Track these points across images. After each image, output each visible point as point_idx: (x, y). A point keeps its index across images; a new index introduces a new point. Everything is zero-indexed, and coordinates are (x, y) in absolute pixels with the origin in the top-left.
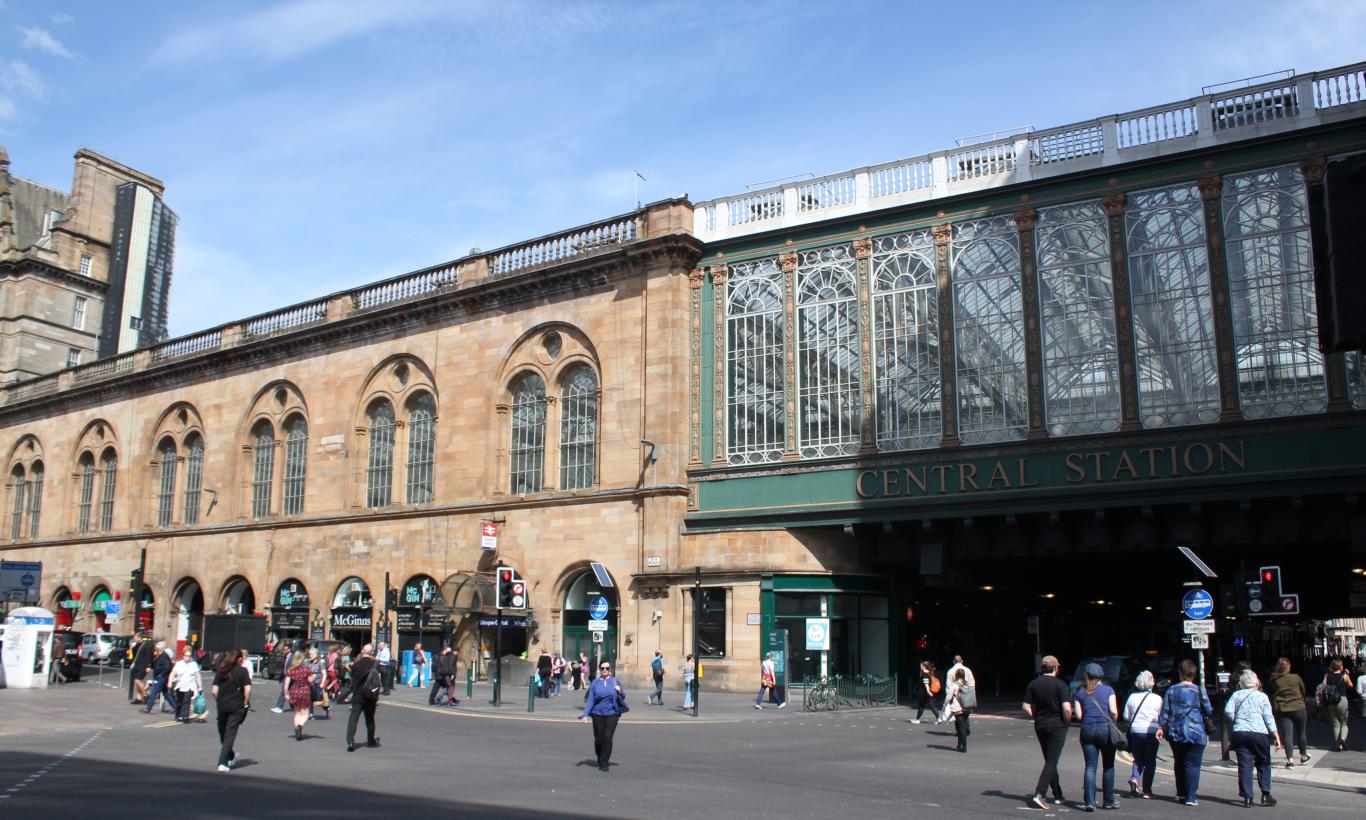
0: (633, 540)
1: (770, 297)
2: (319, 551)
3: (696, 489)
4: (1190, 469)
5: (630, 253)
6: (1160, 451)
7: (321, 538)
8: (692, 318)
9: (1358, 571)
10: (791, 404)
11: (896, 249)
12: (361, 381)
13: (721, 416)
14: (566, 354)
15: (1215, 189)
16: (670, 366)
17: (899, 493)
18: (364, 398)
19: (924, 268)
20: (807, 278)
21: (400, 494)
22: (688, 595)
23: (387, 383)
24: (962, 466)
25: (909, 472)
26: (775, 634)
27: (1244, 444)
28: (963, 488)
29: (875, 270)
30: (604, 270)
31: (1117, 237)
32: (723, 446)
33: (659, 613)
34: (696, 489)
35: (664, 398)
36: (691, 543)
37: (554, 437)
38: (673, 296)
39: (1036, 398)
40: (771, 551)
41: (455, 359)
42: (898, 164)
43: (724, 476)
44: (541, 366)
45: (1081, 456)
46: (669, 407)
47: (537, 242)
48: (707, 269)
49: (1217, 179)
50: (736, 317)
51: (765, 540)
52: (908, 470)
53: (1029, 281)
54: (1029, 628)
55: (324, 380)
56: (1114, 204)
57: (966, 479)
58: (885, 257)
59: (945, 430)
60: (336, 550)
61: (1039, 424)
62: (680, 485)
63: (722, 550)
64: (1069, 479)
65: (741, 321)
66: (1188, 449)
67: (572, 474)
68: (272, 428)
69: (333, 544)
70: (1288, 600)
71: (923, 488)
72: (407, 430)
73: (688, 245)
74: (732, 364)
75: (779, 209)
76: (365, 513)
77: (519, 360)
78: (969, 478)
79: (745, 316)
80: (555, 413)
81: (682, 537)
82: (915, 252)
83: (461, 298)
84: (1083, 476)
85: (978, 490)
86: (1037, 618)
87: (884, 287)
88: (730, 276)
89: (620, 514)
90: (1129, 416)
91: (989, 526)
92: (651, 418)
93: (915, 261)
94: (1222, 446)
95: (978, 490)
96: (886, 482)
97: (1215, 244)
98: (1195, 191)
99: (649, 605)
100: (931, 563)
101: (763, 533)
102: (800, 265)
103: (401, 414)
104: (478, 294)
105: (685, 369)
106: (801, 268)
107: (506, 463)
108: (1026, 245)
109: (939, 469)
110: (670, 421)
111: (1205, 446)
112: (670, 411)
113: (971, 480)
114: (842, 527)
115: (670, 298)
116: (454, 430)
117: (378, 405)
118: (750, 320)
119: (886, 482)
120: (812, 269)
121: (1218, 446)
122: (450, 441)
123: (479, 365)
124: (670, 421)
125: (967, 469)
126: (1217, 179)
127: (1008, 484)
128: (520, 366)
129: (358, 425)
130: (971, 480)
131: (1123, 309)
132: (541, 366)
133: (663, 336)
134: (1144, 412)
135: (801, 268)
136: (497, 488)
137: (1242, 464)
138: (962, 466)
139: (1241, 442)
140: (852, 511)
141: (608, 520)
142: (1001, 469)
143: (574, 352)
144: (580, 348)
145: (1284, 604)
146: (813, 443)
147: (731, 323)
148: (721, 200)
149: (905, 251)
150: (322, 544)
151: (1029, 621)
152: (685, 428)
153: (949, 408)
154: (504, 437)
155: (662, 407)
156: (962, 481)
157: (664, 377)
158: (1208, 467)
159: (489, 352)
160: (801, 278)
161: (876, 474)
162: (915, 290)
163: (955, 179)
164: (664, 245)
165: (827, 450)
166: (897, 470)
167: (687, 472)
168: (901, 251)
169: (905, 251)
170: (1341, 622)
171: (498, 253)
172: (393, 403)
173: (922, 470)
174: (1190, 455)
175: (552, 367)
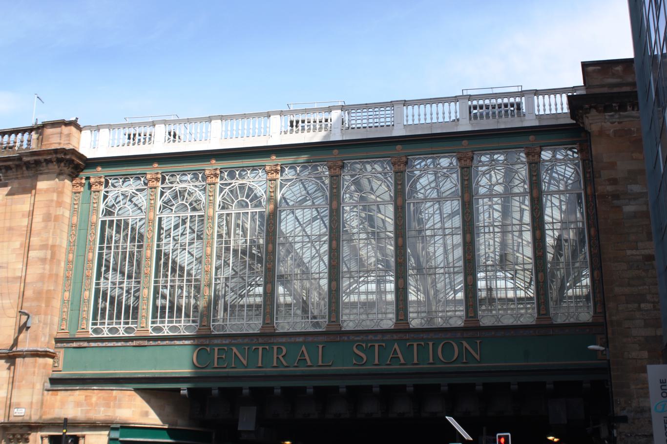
3: (61, 354)
4: (442, 359)
8: (72, 215)
15: (468, 160)
16: (49, 252)
25: (235, 350)
27: (248, 348)
28: (275, 364)
29: (161, 197)
31: (399, 187)
34: (61, 354)
35: (42, 278)
36: (53, 398)
38: (58, 197)
39: (268, 303)
40: (120, 407)
45: (364, 345)
48: (88, 178)
50: (108, 218)
53: (536, 202)
57: (278, 358)
59: (330, 317)
63: (78, 404)
64: (354, 362)
66: (444, 342)
78: (280, 357)
81: (46, 392)
91: (292, 395)
92: (29, 293)
94: (465, 344)
101: (115, 392)
102: (163, 183)
105: (62, 256)
111: (453, 343)
119: (216, 356)
120: (230, 184)
124: (45, 297)
125: (279, 350)
126: (470, 154)
127: (309, 363)
131: (468, 236)
134: (411, 315)
135: (164, 186)
138: (275, 348)
146: (117, 323)
147: (103, 223)
148: (275, 113)
152: (57, 303)
153: (268, 303)
155: (39, 285)
160: (162, 193)
161: (208, 349)
166: (226, 348)
167: (55, 339)
169: (244, 182)
173: (245, 348)
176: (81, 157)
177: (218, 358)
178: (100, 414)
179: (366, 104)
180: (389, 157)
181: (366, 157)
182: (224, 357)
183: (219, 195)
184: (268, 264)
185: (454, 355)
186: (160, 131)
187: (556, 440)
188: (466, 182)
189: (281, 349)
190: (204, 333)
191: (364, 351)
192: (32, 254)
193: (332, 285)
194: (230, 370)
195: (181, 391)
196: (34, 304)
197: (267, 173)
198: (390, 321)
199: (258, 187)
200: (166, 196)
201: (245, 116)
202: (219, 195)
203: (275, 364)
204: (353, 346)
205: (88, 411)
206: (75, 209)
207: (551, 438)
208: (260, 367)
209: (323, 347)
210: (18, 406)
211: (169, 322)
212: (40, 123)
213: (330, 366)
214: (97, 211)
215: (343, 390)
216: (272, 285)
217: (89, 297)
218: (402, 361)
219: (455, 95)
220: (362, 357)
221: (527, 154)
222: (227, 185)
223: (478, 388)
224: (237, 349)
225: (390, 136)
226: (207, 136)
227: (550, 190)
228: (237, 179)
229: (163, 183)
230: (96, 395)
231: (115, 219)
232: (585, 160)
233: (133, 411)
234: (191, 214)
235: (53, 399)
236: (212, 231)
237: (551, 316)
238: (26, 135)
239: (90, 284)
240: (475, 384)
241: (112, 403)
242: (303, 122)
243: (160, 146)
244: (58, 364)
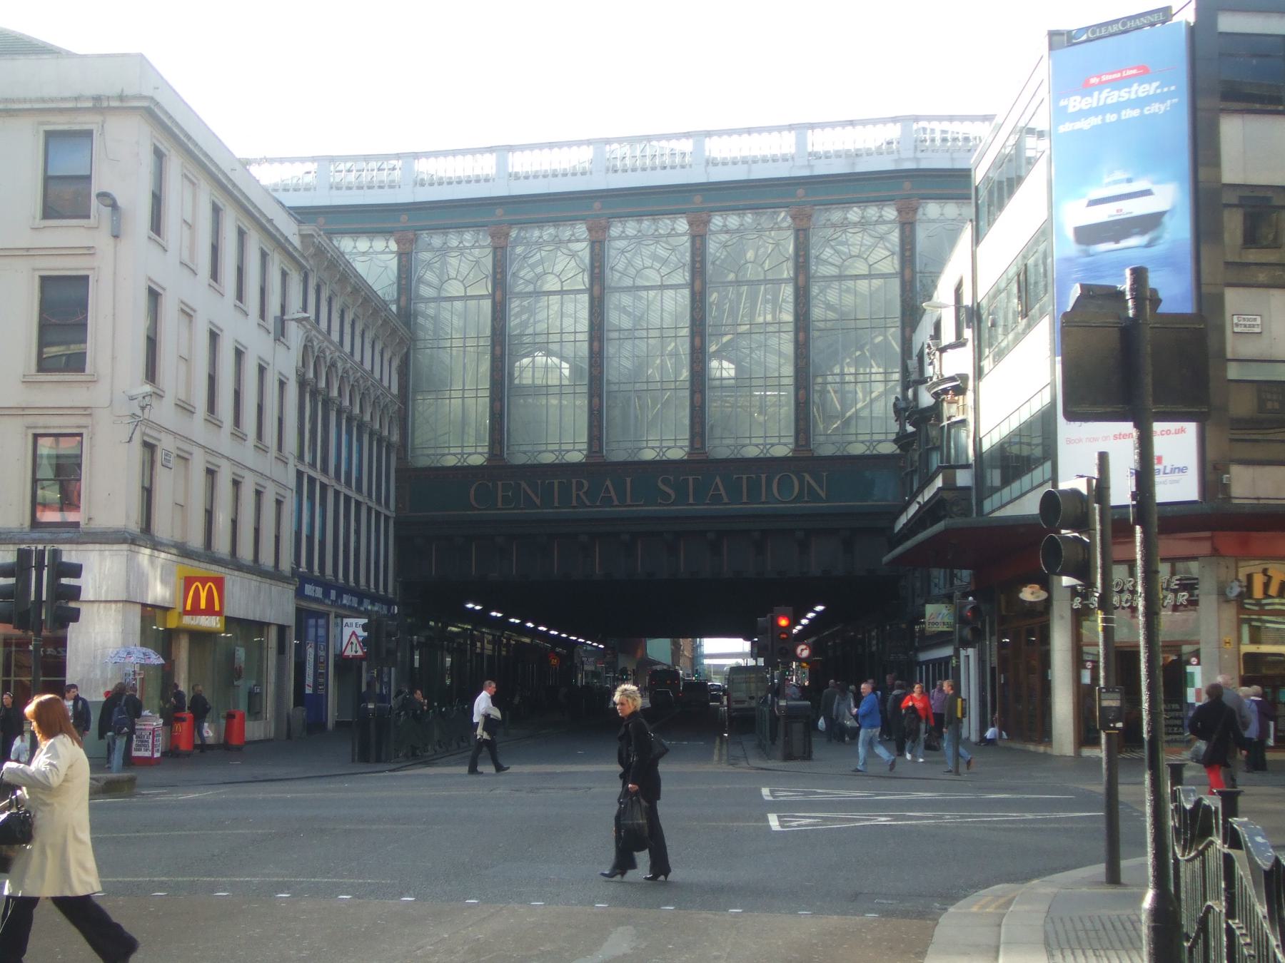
6: (563, 483)
9: (478, 608)
17: (642, 503)
24: (574, 481)
25: (524, 485)
28: (574, 503)
39: (596, 423)
49: (603, 222)
57: (578, 495)
64: (659, 501)
66: (778, 477)
78: (581, 493)
85: (589, 506)
90: (696, 446)
94: (807, 477)
95: (589, 506)
96: (500, 494)
98: (393, 246)
113: (583, 497)
121: (803, 477)
125: (580, 486)
130: (583, 497)
139: (539, 482)
140: (58, 523)
156: (574, 495)
158: (793, 497)
174: (779, 484)
177: (503, 496)
187: (478, 608)
188: (596, 271)
189: (583, 484)
193: (695, 399)
198: (862, 445)
203: (574, 503)
204: (589, 488)
207: (470, 606)
209: (766, 477)
216: (600, 399)
217: (501, 411)
218: (616, 503)
221: (590, 230)
227: (819, 274)
232: (798, 230)
237: (707, 449)
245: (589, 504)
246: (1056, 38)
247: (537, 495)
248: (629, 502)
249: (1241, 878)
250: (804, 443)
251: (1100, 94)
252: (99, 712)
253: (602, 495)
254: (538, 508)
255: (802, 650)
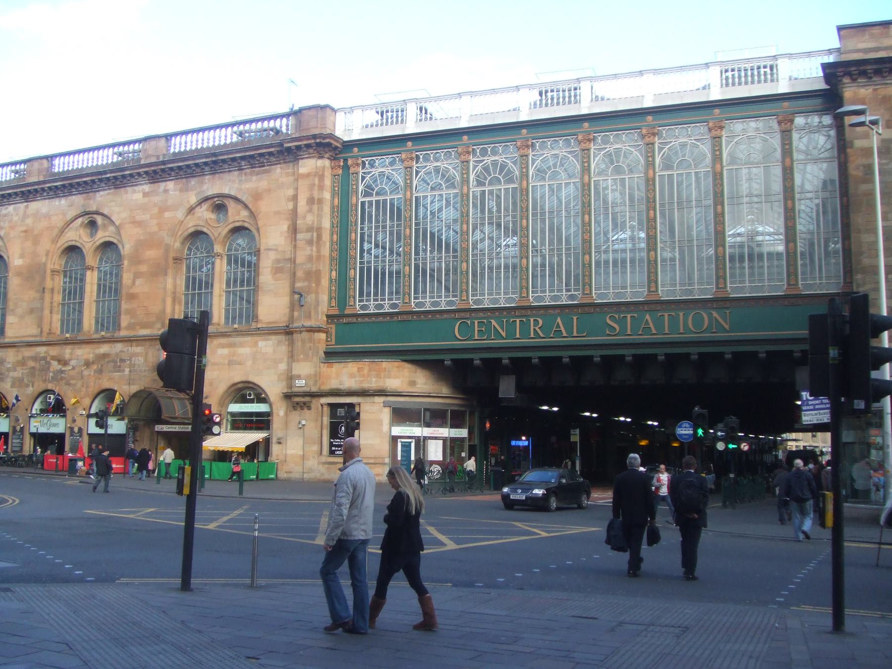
0: (283, 367)
1: (394, 185)
2: (18, 368)
4: (694, 330)
5: (286, 145)
7: (20, 358)
8: (333, 197)
10: (352, 271)
11: (612, 144)
12: (56, 231)
13: (465, 267)
14: (231, 220)
16: (315, 234)
17: (485, 338)
18: (59, 244)
19: (510, 172)
20: (368, 177)
21: (220, 317)
22: (326, 410)
23: (77, 235)
24: (532, 320)
25: (494, 322)
26: (796, 441)
28: (532, 335)
29: (416, 176)
30: (312, 147)
31: (787, 147)
32: (354, 297)
33: (304, 422)
35: (310, 258)
36: (329, 370)
37: (220, 284)
38: (319, 180)
40: (389, 377)
41: (138, 218)
42: (682, 68)
43: (354, 320)
44: (210, 228)
45: (617, 316)
46: (314, 266)
47: (209, 129)
48: (346, 160)
50: (367, 199)
51: (385, 368)
52: (493, 321)
54: (572, 437)
55: (23, 228)
56: (464, 153)
58: (369, 173)
59: (649, 287)
60: (33, 368)
61: (588, 292)
62: (321, 326)
63: (352, 376)
64: (608, 332)
65: (370, 203)
67: (73, 324)
68: (84, 255)
69: (31, 364)
70: (217, 416)
71: (504, 334)
72: (96, 273)
73: (332, 142)
74: (362, 235)
75: (402, 120)
76: (59, 338)
77: (191, 225)
78: (537, 328)
79: (374, 199)
80: (221, 267)
81: (322, 364)
82: (504, 160)
83: (152, 168)
84: (617, 332)
85: (543, 338)
86: (578, 431)
87: (480, 183)
88: (363, 168)
89: (268, 346)
90: (720, 286)
91: (550, 364)
92: (300, 274)
93: (503, 167)
94: (715, 314)
95: (543, 338)
96: (476, 329)
97: (842, 160)
99: (295, 416)
100: (507, 388)
102: (363, 168)
103: (91, 259)
104: (159, 167)
105: (326, 237)
106: (418, 165)
107: (180, 304)
108: (716, 149)
109: (516, 321)
110: (313, 276)
111: (702, 313)
112: (314, 269)
114: (443, 361)
115: (317, 182)
116: (137, 275)
117: (73, 250)
118: (378, 202)
119: (476, 329)
120: (426, 166)
122: (134, 283)
123: (159, 224)
124: (313, 276)
127: (654, 331)
128: (192, 227)
129: (52, 267)
131: (789, 202)
132: (210, 228)
133: (310, 211)
135: (418, 165)
136: (50, 330)
137: (727, 327)
138: (532, 320)
139: (505, 320)
141: (263, 350)
142: (650, 321)
143: (237, 218)
144: (244, 213)
145: (214, 418)
146: (367, 301)
147: (363, 203)
148: (524, 86)
149: (496, 158)
150: (22, 363)
151: (572, 432)
152: (325, 282)
154: (178, 282)
155: (309, 266)
157: (310, 242)
159: (167, 214)
160: (363, 178)
161: (469, 322)
162: (388, 198)
163: (421, 120)
164: (313, 141)
165: (449, 303)
166: (485, 321)
167: (326, 315)
168: (493, 158)
169: (496, 158)
170: (794, 435)
171: (176, 134)
172: (84, 250)
175: (220, 230)
176: (337, 139)
178: (373, 383)
179: (681, 67)
180: (774, 115)
181: (808, 111)
182: (483, 329)
183: (659, 154)
184: (718, 226)
185: (704, 323)
186: (412, 111)
190: (464, 307)
191: (616, 322)
192: (300, 236)
193: (718, 251)
194: (677, 336)
195: (503, 361)
196: (306, 284)
197: (580, 142)
199: (701, 145)
200: (421, 176)
201: (494, 91)
202: (659, 154)
203: (532, 335)
205: (361, 382)
206: (717, 155)
208: (532, 338)
210: (299, 377)
211: (375, 300)
212: (296, 108)
213: (484, 340)
214: (357, 192)
215: (661, 358)
218: (565, 334)
219: (576, 78)
220: (615, 328)
221: (779, 123)
222: (600, 150)
223: (727, 356)
224: (718, 314)
225: (514, 120)
226: (402, 120)
228: (489, 156)
229: (417, 163)
230: (365, 365)
231: (487, 189)
233: (402, 381)
234: (376, 199)
235: (329, 371)
236: (721, 188)
238: (285, 120)
239: (355, 263)
240: (473, 359)
241: (382, 374)
242: (558, 91)
243: (411, 127)
244: (331, 339)
245: (543, 336)
246: (842, 33)
247: (727, 324)
248: (575, 334)
249: (490, 593)
250: (794, 283)
251: (180, 150)
252: (643, 542)
253: (554, 329)
254: (505, 339)
255: (745, 446)
